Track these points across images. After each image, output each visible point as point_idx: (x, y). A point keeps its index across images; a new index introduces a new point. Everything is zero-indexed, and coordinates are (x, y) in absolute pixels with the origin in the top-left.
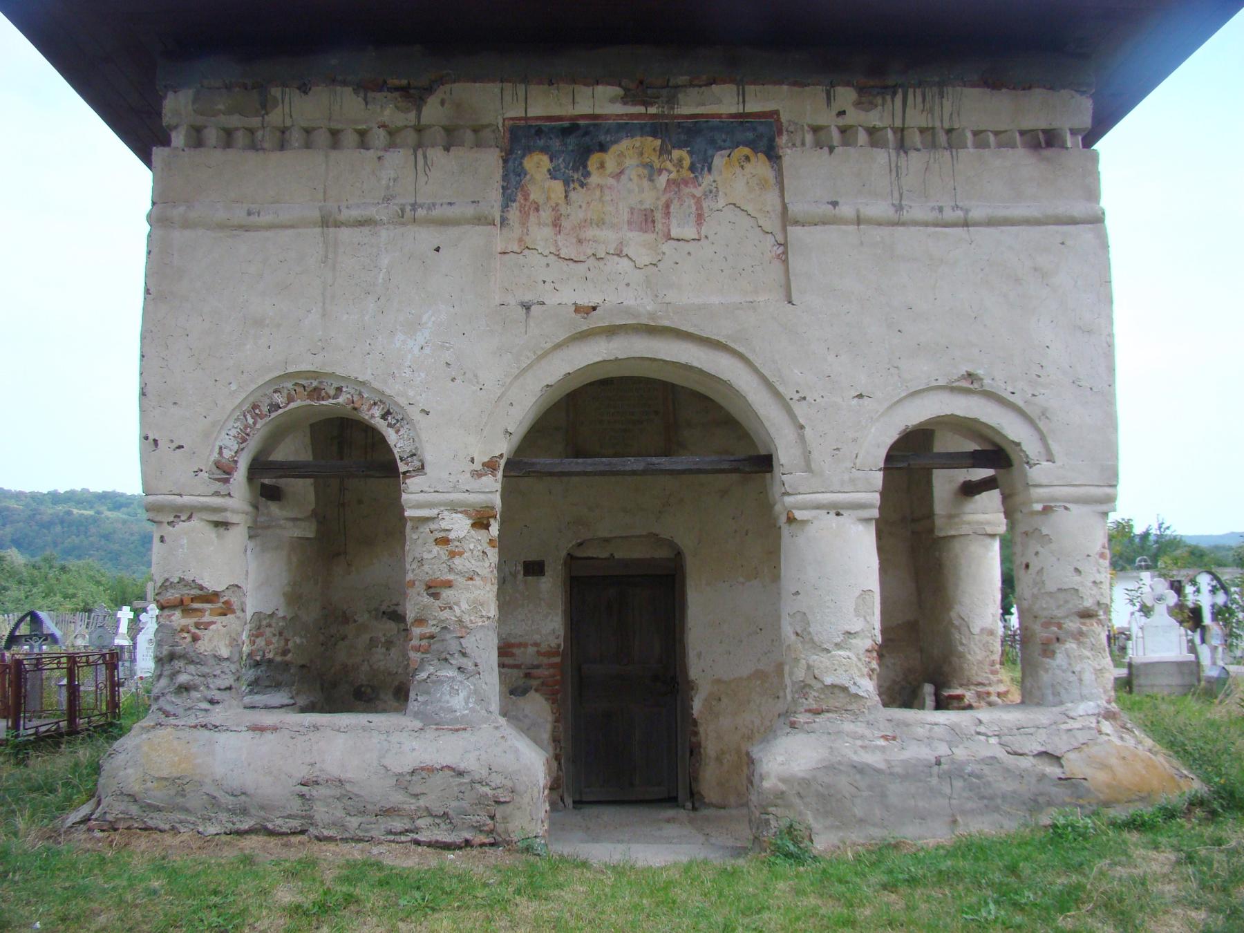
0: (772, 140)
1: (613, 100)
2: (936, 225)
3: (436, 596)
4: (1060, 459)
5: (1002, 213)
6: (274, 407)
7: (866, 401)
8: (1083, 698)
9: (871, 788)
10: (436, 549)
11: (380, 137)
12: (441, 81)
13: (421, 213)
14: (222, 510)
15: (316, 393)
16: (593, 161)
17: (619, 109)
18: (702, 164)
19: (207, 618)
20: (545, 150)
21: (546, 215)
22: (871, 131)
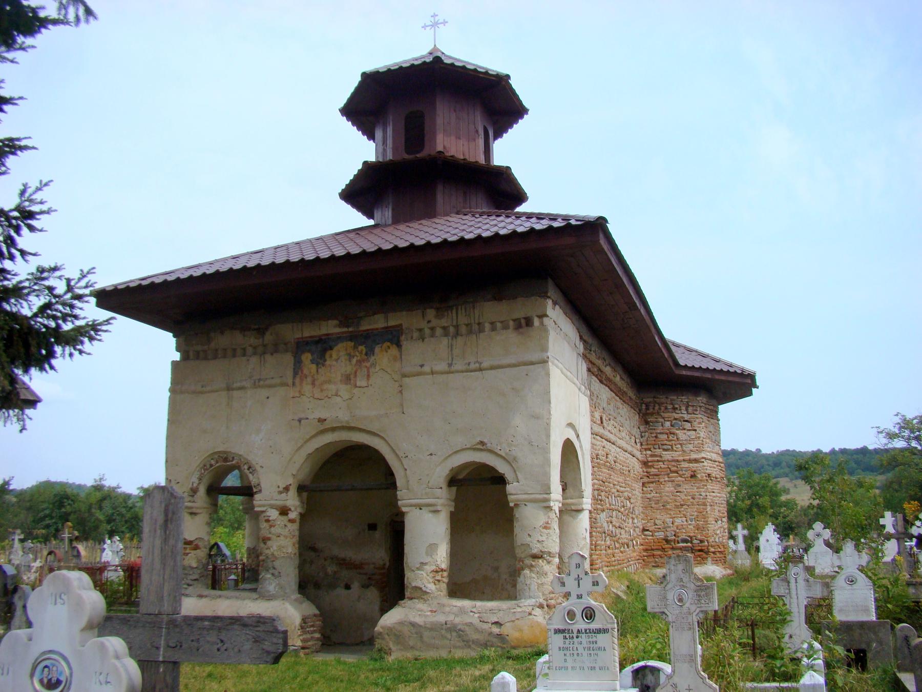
0: (399, 338)
1: (335, 327)
3: (265, 543)
4: (522, 481)
5: (496, 363)
6: (211, 466)
8: (530, 597)
9: (416, 633)
11: (250, 350)
13: (262, 383)
14: (191, 508)
15: (226, 460)
16: (327, 356)
17: (338, 330)
18: (370, 352)
20: (309, 351)
21: (309, 380)
22: (444, 328)
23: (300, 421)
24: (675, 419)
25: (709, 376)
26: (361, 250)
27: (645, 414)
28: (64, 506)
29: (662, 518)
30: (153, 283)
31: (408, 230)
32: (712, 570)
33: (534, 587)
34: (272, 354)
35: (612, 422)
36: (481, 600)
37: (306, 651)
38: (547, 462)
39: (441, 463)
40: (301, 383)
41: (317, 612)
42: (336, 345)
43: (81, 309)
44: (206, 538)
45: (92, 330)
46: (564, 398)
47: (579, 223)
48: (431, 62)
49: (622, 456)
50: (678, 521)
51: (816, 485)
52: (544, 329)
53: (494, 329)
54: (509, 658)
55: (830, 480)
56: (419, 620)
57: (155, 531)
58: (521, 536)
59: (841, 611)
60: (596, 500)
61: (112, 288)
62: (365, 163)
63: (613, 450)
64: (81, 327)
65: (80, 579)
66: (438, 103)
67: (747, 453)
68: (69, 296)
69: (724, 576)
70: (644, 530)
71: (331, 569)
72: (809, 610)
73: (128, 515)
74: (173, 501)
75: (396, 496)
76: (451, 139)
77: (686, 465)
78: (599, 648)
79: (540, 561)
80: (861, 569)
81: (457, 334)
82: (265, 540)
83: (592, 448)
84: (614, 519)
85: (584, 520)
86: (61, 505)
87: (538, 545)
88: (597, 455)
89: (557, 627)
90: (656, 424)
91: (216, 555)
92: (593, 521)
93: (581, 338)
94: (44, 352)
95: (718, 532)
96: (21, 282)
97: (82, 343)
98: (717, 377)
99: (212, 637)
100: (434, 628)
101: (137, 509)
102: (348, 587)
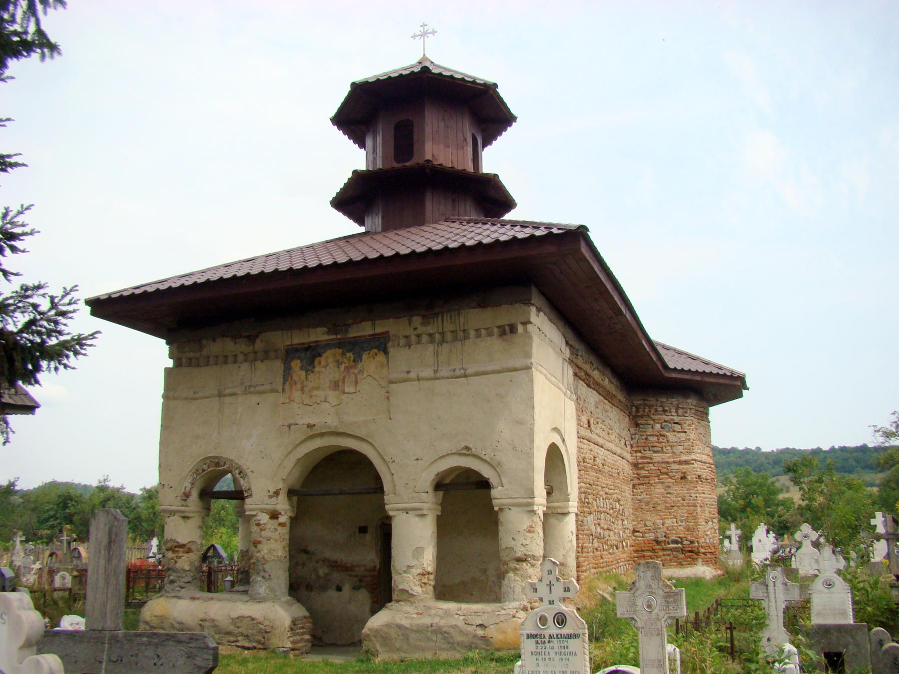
0: (385, 345)
1: (323, 334)
2: (452, 378)
3: (256, 547)
6: (204, 470)
7: (420, 461)
8: (514, 600)
9: (403, 635)
10: (256, 528)
11: (241, 357)
12: (260, 333)
13: (252, 389)
14: (183, 512)
15: (217, 465)
17: (326, 337)
18: (358, 359)
19: (180, 554)
20: (299, 358)
21: (299, 386)
22: (430, 335)
23: (289, 426)
24: (666, 421)
25: (698, 378)
26: (348, 259)
27: (635, 417)
28: (68, 507)
29: (652, 519)
30: (145, 292)
31: (396, 238)
32: (704, 571)
33: (518, 590)
34: (262, 361)
35: (600, 425)
36: (468, 602)
37: (297, 652)
38: (531, 467)
39: (427, 467)
40: (291, 390)
41: (307, 614)
42: (325, 352)
43: (65, 325)
44: (199, 542)
45: (78, 344)
46: (549, 400)
47: (561, 232)
48: (419, 72)
49: (611, 458)
50: (668, 522)
51: (804, 486)
52: (528, 336)
53: (478, 336)
54: (492, 660)
55: (820, 481)
56: (405, 623)
57: (100, 551)
58: (505, 540)
59: (818, 614)
60: (582, 502)
61: (106, 297)
62: (355, 172)
63: (601, 453)
64: (66, 342)
65: (21, 600)
66: (426, 112)
67: (747, 451)
68: (53, 312)
69: (714, 576)
70: (634, 531)
71: (322, 572)
72: (792, 612)
73: (132, 516)
74: (116, 523)
75: (383, 499)
76: (440, 145)
77: (675, 467)
78: (571, 653)
79: (524, 564)
80: (839, 572)
81: (443, 341)
82: (256, 543)
83: (579, 451)
84: (602, 522)
85: (570, 524)
86: (65, 506)
87: (523, 549)
88: (584, 459)
89: (529, 632)
90: (647, 427)
91: (212, 557)
92: (580, 524)
93: (567, 343)
94: (30, 367)
95: (709, 533)
96: (7, 299)
97: (68, 357)
98: (707, 379)
99: (150, 652)
100: (420, 630)
101: (139, 510)
102: (339, 589)
